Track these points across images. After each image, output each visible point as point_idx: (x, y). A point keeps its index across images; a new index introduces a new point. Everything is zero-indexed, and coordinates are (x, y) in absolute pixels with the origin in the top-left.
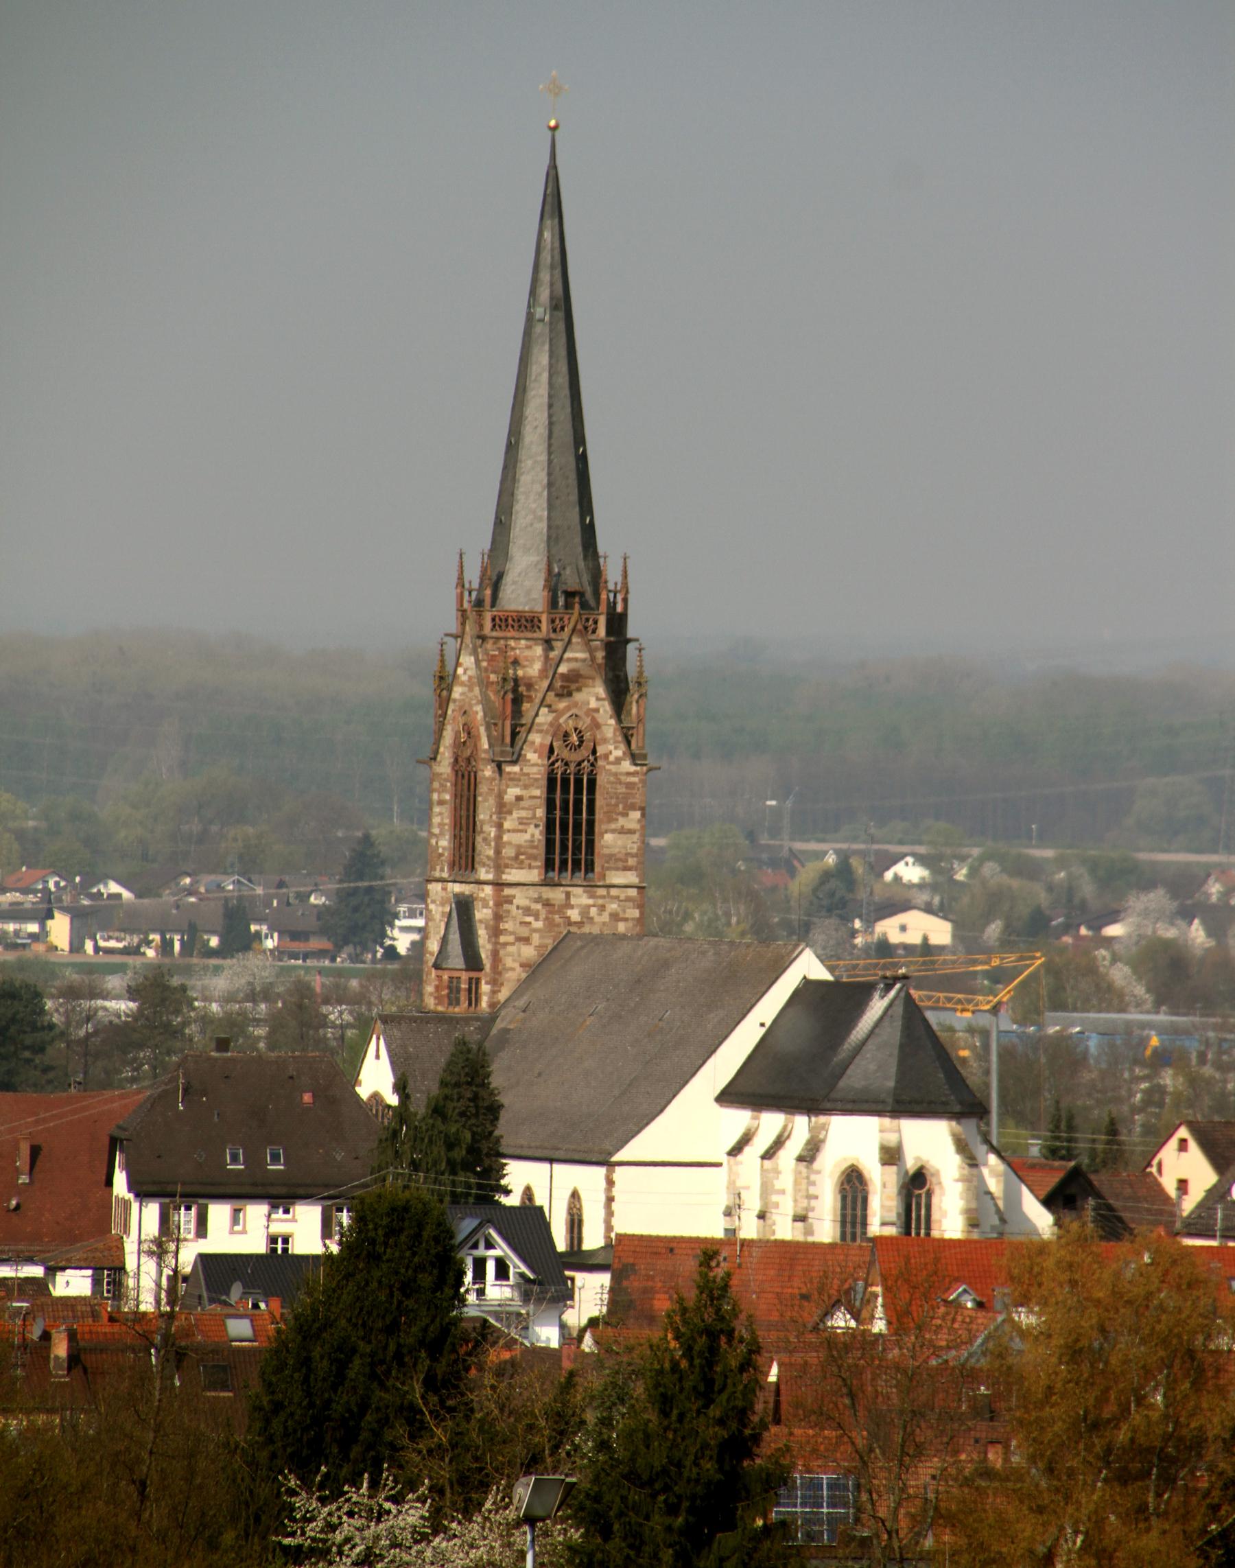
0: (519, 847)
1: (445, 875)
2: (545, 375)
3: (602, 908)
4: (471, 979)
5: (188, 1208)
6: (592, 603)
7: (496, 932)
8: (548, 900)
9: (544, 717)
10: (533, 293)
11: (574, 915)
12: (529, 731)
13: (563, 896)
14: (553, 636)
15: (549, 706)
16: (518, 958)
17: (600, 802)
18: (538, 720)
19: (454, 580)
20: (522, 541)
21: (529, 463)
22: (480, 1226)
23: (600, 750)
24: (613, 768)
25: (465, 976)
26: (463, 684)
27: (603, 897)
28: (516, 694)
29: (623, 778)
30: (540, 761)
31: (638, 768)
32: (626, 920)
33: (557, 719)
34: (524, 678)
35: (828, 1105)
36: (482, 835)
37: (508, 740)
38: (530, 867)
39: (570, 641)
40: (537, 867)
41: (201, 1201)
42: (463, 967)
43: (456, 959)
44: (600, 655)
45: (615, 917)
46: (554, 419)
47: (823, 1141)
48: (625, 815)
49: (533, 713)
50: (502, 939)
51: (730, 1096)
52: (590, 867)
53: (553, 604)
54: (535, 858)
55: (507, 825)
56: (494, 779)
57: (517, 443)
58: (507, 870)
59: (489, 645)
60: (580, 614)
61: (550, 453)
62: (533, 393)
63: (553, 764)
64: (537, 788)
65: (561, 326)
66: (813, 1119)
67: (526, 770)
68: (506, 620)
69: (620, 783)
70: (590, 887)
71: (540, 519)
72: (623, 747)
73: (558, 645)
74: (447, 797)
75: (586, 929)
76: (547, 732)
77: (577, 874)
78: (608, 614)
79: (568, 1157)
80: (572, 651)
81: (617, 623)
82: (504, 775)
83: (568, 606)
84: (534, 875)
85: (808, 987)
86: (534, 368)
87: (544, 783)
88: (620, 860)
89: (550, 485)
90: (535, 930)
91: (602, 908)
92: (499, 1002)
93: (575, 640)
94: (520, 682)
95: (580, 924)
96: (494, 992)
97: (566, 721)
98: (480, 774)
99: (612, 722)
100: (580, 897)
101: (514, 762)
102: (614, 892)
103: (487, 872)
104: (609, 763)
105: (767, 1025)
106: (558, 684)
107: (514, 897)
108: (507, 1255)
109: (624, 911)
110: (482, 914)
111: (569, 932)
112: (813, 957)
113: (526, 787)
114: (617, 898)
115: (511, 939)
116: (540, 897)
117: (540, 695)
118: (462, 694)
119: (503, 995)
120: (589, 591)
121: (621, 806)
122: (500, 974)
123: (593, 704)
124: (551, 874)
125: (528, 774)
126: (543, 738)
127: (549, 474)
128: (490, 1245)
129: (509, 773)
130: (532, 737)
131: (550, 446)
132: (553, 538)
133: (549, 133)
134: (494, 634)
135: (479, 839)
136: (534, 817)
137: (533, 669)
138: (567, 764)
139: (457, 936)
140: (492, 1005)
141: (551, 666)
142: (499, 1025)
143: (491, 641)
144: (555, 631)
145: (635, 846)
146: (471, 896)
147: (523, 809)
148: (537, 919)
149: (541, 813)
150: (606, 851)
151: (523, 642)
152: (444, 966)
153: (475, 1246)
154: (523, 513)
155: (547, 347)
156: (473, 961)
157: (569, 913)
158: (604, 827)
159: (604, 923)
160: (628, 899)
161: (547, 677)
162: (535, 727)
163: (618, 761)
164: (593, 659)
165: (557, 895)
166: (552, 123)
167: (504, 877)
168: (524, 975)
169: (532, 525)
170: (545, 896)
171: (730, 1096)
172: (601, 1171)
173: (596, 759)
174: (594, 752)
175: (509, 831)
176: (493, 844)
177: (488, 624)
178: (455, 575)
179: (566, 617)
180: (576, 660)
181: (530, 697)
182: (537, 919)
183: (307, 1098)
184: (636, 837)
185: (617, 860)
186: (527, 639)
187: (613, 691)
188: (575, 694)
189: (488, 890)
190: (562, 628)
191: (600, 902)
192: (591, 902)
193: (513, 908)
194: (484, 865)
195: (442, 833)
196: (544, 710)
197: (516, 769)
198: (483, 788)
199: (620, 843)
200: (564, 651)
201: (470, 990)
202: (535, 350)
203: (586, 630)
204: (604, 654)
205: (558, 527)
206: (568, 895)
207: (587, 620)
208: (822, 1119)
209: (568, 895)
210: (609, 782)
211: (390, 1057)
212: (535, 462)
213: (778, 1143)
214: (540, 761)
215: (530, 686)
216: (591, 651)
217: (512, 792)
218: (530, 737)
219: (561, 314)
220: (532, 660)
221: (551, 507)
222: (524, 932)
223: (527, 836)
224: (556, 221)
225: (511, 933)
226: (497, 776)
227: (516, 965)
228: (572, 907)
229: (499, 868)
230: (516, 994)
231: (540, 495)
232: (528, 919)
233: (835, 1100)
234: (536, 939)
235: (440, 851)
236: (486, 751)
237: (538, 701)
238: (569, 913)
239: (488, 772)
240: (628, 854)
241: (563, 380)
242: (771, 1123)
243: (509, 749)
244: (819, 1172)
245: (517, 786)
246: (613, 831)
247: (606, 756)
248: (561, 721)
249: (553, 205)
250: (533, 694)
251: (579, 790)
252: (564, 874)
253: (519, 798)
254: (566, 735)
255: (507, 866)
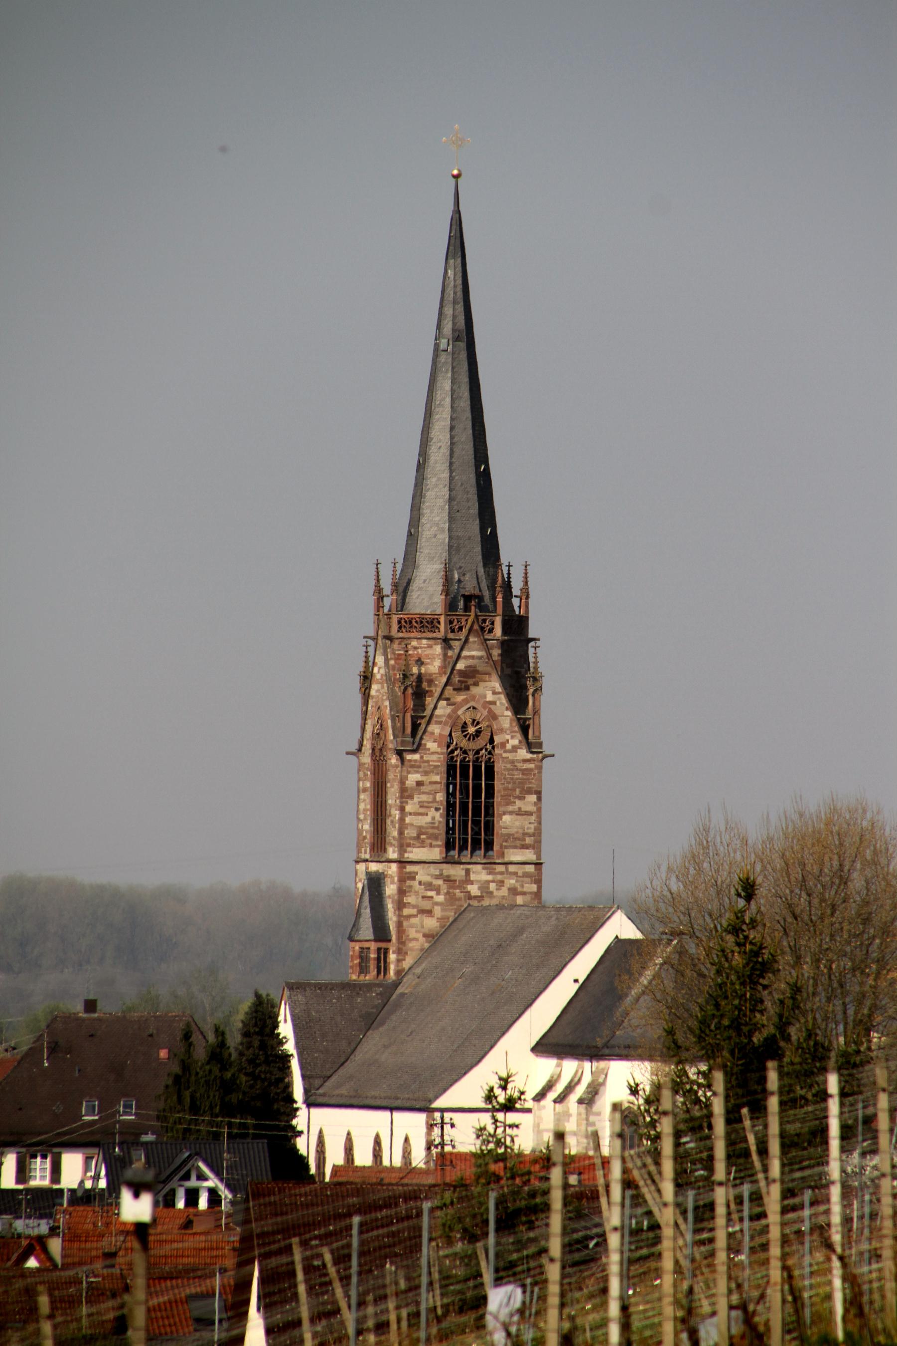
0: (420, 827)
1: (367, 856)
2: (448, 400)
3: (501, 883)
4: (379, 949)
5: (44, 1157)
6: (491, 607)
7: (400, 905)
8: (448, 876)
9: (443, 709)
10: (439, 327)
11: (474, 890)
12: (429, 723)
13: (463, 873)
14: (451, 636)
15: (448, 699)
16: (418, 929)
17: (498, 785)
18: (437, 712)
19: (372, 588)
20: (427, 551)
21: (434, 480)
22: (190, 1157)
23: (497, 739)
24: (510, 756)
25: (373, 946)
26: (378, 683)
27: (501, 873)
28: (418, 690)
29: (519, 765)
30: (439, 750)
31: (535, 756)
32: (524, 894)
33: (455, 711)
34: (426, 673)
35: (607, 1051)
36: (391, 818)
37: (409, 730)
38: (431, 846)
39: (466, 641)
40: (438, 846)
41: (56, 1150)
42: (372, 937)
43: (366, 931)
44: (496, 652)
45: (513, 891)
46: (456, 439)
47: (603, 1084)
48: (522, 798)
49: (432, 706)
50: (406, 912)
51: (549, 1046)
52: (489, 846)
53: (451, 606)
54: (436, 838)
55: (408, 808)
56: (397, 766)
57: (424, 461)
58: (409, 849)
59: (396, 645)
60: (477, 616)
61: (451, 471)
62: (437, 417)
63: (452, 752)
64: (437, 774)
65: (463, 355)
66: (595, 1064)
67: (426, 758)
68: (411, 622)
69: (517, 770)
70: (489, 865)
71: (443, 530)
72: (519, 736)
73: (456, 645)
74: (368, 784)
75: (486, 902)
76: (446, 724)
77: (478, 852)
78: (504, 615)
79: (408, 1105)
80: (470, 650)
81: (517, 627)
82: (406, 763)
83: (467, 609)
84: (436, 853)
85: (619, 944)
86: (439, 392)
87: (444, 769)
88: (519, 839)
89: (451, 499)
90: (437, 904)
91: (501, 883)
92: (403, 970)
93: (471, 639)
94: (424, 679)
95: (479, 898)
96: (398, 961)
97: (464, 713)
98: (388, 762)
99: (509, 713)
100: (480, 874)
101: (414, 751)
102: (512, 868)
103: (394, 852)
104: (505, 752)
105: (581, 982)
106: (456, 679)
107: (417, 873)
108: (217, 1186)
109: (522, 886)
110: (390, 889)
111: (469, 905)
112: (625, 918)
113: (426, 773)
114: (516, 874)
115: (414, 911)
116: (441, 874)
117: (439, 690)
118: (378, 691)
119: (406, 964)
120: (486, 594)
121: (518, 790)
122: (404, 943)
123: (490, 697)
124: (452, 853)
125: (428, 761)
126: (442, 729)
127: (450, 490)
128: (202, 1177)
129: (410, 761)
130: (431, 728)
131: (451, 464)
132: (454, 547)
133: (453, 180)
134: (400, 635)
135: (388, 822)
136: (434, 801)
137: (434, 666)
138: (465, 752)
139: (368, 910)
140: (398, 973)
141: (450, 665)
142: (400, 990)
143: (397, 642)
144: (453, 631)
145: (532, 826)
146: (383, 873)
147: (423, 793)
148: (438, 893)
149: (441, 797)
150: (504, 831)
151: (424, 641)
152: (356, 938)
153: (187, 1177)
154: (428, 525)
155: (449, 375)
156: (381, 933)
157: (469, 887)
158: (502, 809)
159: (503, 897)
160: (526, 875)
161: (445, 673)
162: (434, 719)
163: (515, 749)
164: (490, 655)
165: (457, 872)
166: (455, 172)
167: (406, 855)
168: (427, 945)
169: (435, 536)
170: (445, 873)
171: (549, 1046)
172: (422, 1117)
173: (493, 748)
174: (492, 741)
175: (410, 814)
176: (397, 825)
177: (395, 627)
178: (373, 582)
179: (463, 619)
180: (473, 657)
181: (431, 691)
182: (438, 893)
183: (163, 1054)
184: (533, 818)
185: (515, 839)
186: (428, 639)
187: (512, 686)
188: (472, 688)
189: (394, 867)
190: (461, 629)
191: (499, 877)
192: (490, 877)
193: (415, 884)
194: (391, 845)
195: (365, 819)
196: (443, 703)
197: (416, 757)
198: (390, 776)
199: (517, 823)
200: (462, 649)
201: (378, 959)
202: (440, 378)
203: (483, 630)
204: (500, 652)
205: (458, 538)
206: (468, 872)
207: (484, 621)
208: (602, 1064)
209: (468, 872)
210: (506, 769)
211: (293, 1021)
212: (439, 479)
213: (570, 1088)
214: (439, 750)
215: (431, 682)
216: (488, 649)
217: (413, 778)
218: (430, 728)
219: (462, 345)
220: (431, 657)
221: (451, 519)
222: (426, 905)
223: (428, 819)
224: (459, 260)
225: (414, 907)
226: (399, 763)
227: (420, 936)
228: (472, 883)
229: (403, 847)
230: (417, 963)
231: (442, 508)
232: (430, 894)
233: (613, 1047)
234: (438, 911)
235: (364, 834)
236: (392, 742)
237: (437, 695)
238: (469, 887)
239: (394, 760)
240: (525, 834)
241: (465, 403)
242: (570, 1067)
243: (410, 739)
244: (599, 1114)
245: (417, 772)
246: (511, 813)
247: (503, 745)
248: (460, 712)
249: (457, 246)
250: (433, 689)
251: (477, 775)
252: (465, 852)
253: (419, 784)
254: (464, 726)
255: (409, 845)
